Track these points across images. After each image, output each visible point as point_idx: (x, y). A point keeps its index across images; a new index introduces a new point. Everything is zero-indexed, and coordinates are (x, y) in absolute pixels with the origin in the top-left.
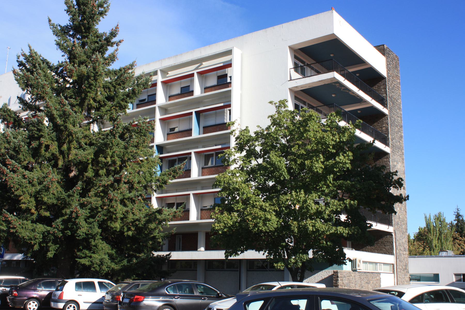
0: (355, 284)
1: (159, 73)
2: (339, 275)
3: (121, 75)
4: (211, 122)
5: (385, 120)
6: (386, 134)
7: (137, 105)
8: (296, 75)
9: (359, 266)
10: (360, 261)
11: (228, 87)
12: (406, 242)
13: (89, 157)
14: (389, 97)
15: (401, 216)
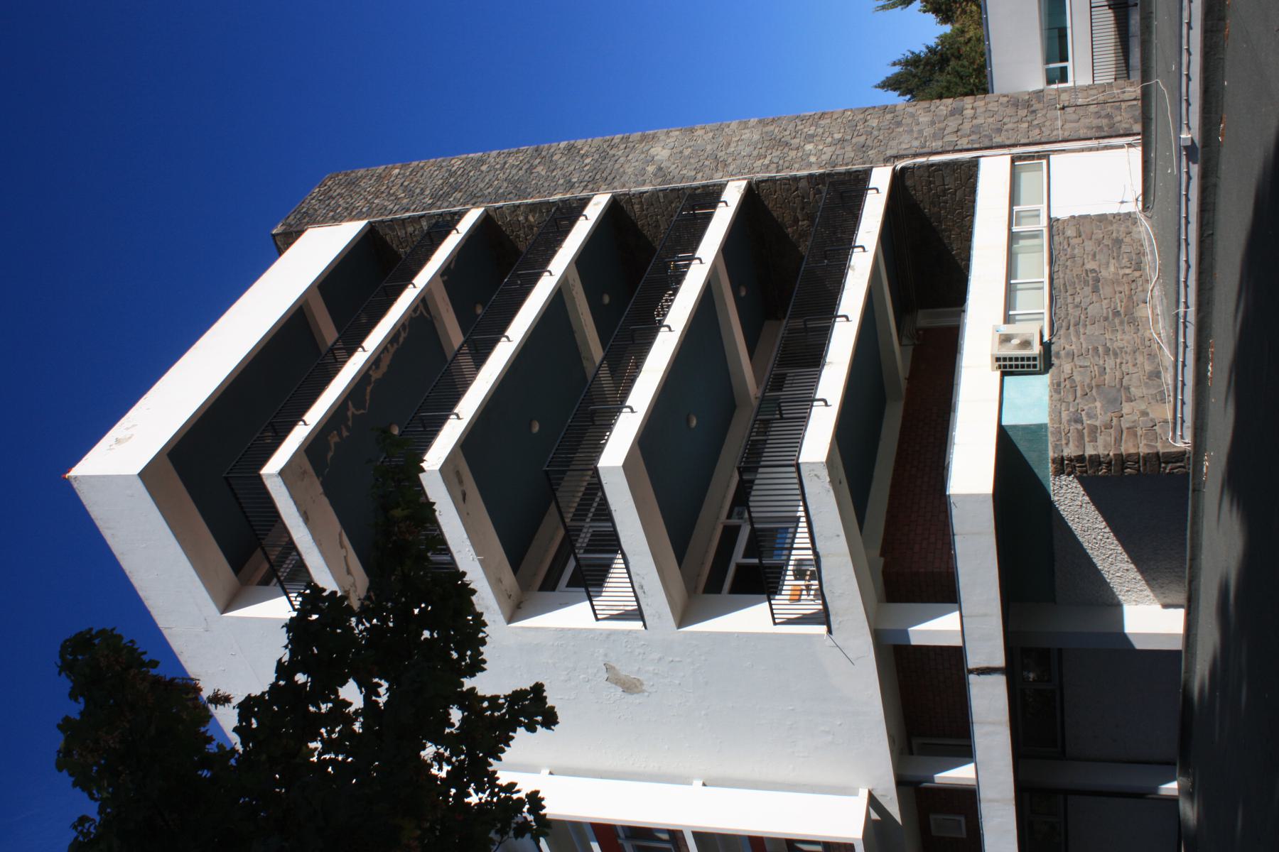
0: (1107, 351)
2: (1070, 451)
5: (503, 216)
6: (549, 211)
9: (1026, 344)
10: (1006, 339)
12: (928, 110)
14: (432, 206)
15: (837, 136)
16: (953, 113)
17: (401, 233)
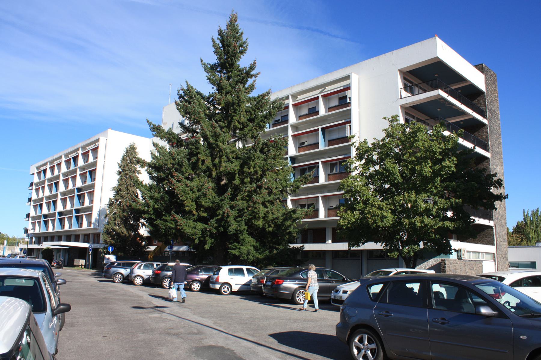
1: (290, 98)
2: (446, 262)
3: (260, 101)
4: (335, 136)
5: (485, 129)
7: (273, 124)
8: (405, 94)
9: (463, 255)
10: (464, 251)
11: (348, 106)
13: (236, 168)
16: (504, 240)
17: (481, 101)
